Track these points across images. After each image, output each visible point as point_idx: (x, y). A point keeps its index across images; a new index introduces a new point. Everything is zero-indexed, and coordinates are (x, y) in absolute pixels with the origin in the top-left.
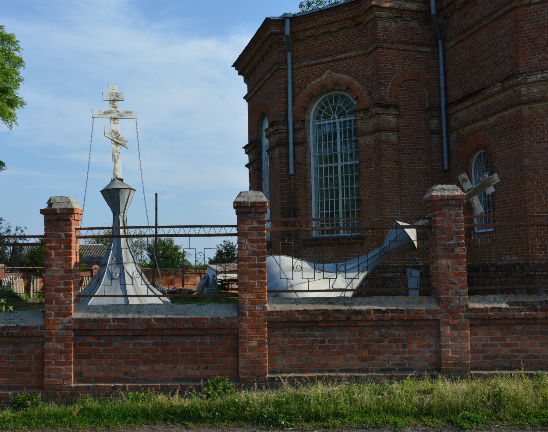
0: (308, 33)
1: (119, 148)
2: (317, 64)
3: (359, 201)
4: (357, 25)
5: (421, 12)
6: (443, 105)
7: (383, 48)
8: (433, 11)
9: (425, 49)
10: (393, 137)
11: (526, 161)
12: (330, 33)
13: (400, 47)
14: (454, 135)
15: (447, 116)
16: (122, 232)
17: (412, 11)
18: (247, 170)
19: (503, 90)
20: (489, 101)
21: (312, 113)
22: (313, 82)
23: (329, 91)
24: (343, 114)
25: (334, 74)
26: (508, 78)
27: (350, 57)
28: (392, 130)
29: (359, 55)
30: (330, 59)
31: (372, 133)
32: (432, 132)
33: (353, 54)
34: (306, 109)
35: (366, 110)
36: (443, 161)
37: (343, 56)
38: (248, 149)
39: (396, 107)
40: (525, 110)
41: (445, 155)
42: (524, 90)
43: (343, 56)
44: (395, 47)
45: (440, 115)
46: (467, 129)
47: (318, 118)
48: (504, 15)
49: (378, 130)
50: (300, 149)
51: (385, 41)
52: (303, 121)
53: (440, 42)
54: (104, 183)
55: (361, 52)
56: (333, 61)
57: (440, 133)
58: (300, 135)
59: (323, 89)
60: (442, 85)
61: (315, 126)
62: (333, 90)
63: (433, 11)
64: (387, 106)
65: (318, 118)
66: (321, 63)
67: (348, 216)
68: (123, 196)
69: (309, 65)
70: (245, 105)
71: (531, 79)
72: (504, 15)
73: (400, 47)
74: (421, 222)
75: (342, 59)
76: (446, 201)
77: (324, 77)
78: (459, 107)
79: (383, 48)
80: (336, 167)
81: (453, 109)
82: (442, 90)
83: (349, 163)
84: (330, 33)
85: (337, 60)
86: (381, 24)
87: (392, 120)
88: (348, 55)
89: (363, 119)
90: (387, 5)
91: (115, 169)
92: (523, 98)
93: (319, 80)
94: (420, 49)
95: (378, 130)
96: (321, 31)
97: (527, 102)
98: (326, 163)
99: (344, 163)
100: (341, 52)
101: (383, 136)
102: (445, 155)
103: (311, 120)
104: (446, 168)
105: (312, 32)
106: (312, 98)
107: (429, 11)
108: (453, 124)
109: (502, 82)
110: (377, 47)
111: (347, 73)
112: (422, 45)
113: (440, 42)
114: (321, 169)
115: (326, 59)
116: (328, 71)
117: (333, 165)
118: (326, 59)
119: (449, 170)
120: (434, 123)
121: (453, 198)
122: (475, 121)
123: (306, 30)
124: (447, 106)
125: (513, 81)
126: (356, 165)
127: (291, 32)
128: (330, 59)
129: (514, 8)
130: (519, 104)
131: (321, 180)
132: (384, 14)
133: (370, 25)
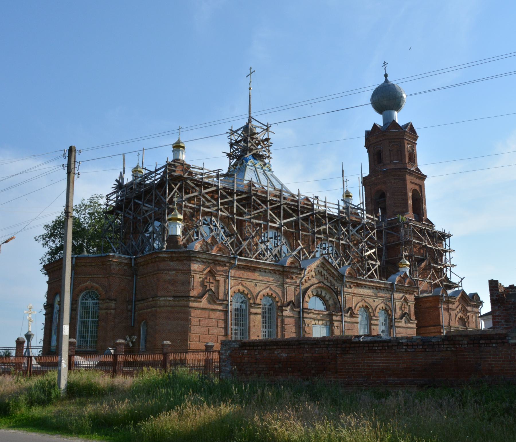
0: (82, 264)
1: (30, 322)
2: (84, 277)
3: (97, 336)
4: (103, 265)
5: (128, 264)
6: (134, 300)
7: (112, 276)
8: (133, 265)
9: (128, 278)
10: (113, 312)
11: (157, 327)
12: (92, 266)
13: (119, 276)
14: (137, 313)
15: (135, 305)
16: (30, 347)
17: (125, 263)
18: (44, 317)
19: (153, 301)
20: (149, 303)
21: (81, 297)
22: (82, 285)
23: (88, 289)
24: (94, 299)
25: (91, 283)
26: (154, 297)
27: (99, 277)
28: (113, 309)
29: (103, 277)
30: (91, 276)
31: (105, 309)
32: (128, 311)
33: (100, 276)
34: (78, 295)
35: (103, 300)
36: (131, 322)
37: (96, 276)
38: (46, 307)
39: (115, 300)
40: (158, 309)
41: (133, 319)
42: (158, 302)
43: (96, 276)
44: (117, 276)
45: (132, 304)
46: (141, 312)
47: (83, 300)
48: (155, 274)
49: (107, 309)
50: (74, 312)
51: (113, 274)
52: (76, 301)
53: (135, 276)
54: (26, 333)
55: (103, 276)
56: (92, 277)
57: (131, 311)
58: (75, 306)
59: (86, 288)
60: (134, 292)
61: (81, 303)
62: (90, 289)
63: (133, 265)
64: (112, 300)
65: (83, 300)
66: (86, 277)
67: (91, 342)
68: (32, 337)
69: (81, 278)
70: (47, 286)
71: (161, 299)
72: (155, 274)
73: (119, 276)
74: (114, 348)
75: (95, 277)
76: (120, 344)
77: (87, 283)
78: (139, 303)
79: (112, 276)
80: (89, 321)
81: (137, 303)
82: (134, 295)
83: (94, 320)
84: (92, 266)
85: (94, 278)
86: (112, 267)
87: (113, 305)
88: (98, 276)
89: (101, 303)
90: (116, 260)
91: (29, 329)
92: (158, 305)
93: (85, 284)
94: (127, 278)
95: (107, 309)
96: (88, 264)
97: (159, 307)
98: (84, 319)
99: (92, 320)
100: (96, 275)
101: (109, 311)
102: (133, 320)
103: (80, 300)
104: (132, 325)
105: (84, 264)
106: (81, 291)
107: (131, 264)
108: (137, 308)
109: (152, 298)
110: (110, 276)
111: (97, 283)
112: (128, 276)
113: (135, 276)
114: (82, 321)
115: (89, 276)
116: (89, 281)
117: (87, 320)
118: (89, 276)
119: (133, 326)
120: (129, 307)
121: (122, 343)
122: (144, 309)
123: (81, 263)
124: (135, 301)
125: (155, 299)
126: (97, 321)
127: (75, 263)
128: (91, 276)
129: (158, 273)
130: (156, 307)
131: (82, 326)
132: (114, 263)
133: (108, 266)
